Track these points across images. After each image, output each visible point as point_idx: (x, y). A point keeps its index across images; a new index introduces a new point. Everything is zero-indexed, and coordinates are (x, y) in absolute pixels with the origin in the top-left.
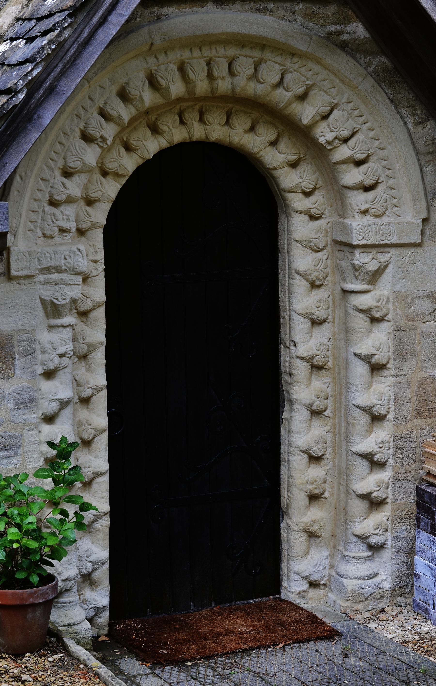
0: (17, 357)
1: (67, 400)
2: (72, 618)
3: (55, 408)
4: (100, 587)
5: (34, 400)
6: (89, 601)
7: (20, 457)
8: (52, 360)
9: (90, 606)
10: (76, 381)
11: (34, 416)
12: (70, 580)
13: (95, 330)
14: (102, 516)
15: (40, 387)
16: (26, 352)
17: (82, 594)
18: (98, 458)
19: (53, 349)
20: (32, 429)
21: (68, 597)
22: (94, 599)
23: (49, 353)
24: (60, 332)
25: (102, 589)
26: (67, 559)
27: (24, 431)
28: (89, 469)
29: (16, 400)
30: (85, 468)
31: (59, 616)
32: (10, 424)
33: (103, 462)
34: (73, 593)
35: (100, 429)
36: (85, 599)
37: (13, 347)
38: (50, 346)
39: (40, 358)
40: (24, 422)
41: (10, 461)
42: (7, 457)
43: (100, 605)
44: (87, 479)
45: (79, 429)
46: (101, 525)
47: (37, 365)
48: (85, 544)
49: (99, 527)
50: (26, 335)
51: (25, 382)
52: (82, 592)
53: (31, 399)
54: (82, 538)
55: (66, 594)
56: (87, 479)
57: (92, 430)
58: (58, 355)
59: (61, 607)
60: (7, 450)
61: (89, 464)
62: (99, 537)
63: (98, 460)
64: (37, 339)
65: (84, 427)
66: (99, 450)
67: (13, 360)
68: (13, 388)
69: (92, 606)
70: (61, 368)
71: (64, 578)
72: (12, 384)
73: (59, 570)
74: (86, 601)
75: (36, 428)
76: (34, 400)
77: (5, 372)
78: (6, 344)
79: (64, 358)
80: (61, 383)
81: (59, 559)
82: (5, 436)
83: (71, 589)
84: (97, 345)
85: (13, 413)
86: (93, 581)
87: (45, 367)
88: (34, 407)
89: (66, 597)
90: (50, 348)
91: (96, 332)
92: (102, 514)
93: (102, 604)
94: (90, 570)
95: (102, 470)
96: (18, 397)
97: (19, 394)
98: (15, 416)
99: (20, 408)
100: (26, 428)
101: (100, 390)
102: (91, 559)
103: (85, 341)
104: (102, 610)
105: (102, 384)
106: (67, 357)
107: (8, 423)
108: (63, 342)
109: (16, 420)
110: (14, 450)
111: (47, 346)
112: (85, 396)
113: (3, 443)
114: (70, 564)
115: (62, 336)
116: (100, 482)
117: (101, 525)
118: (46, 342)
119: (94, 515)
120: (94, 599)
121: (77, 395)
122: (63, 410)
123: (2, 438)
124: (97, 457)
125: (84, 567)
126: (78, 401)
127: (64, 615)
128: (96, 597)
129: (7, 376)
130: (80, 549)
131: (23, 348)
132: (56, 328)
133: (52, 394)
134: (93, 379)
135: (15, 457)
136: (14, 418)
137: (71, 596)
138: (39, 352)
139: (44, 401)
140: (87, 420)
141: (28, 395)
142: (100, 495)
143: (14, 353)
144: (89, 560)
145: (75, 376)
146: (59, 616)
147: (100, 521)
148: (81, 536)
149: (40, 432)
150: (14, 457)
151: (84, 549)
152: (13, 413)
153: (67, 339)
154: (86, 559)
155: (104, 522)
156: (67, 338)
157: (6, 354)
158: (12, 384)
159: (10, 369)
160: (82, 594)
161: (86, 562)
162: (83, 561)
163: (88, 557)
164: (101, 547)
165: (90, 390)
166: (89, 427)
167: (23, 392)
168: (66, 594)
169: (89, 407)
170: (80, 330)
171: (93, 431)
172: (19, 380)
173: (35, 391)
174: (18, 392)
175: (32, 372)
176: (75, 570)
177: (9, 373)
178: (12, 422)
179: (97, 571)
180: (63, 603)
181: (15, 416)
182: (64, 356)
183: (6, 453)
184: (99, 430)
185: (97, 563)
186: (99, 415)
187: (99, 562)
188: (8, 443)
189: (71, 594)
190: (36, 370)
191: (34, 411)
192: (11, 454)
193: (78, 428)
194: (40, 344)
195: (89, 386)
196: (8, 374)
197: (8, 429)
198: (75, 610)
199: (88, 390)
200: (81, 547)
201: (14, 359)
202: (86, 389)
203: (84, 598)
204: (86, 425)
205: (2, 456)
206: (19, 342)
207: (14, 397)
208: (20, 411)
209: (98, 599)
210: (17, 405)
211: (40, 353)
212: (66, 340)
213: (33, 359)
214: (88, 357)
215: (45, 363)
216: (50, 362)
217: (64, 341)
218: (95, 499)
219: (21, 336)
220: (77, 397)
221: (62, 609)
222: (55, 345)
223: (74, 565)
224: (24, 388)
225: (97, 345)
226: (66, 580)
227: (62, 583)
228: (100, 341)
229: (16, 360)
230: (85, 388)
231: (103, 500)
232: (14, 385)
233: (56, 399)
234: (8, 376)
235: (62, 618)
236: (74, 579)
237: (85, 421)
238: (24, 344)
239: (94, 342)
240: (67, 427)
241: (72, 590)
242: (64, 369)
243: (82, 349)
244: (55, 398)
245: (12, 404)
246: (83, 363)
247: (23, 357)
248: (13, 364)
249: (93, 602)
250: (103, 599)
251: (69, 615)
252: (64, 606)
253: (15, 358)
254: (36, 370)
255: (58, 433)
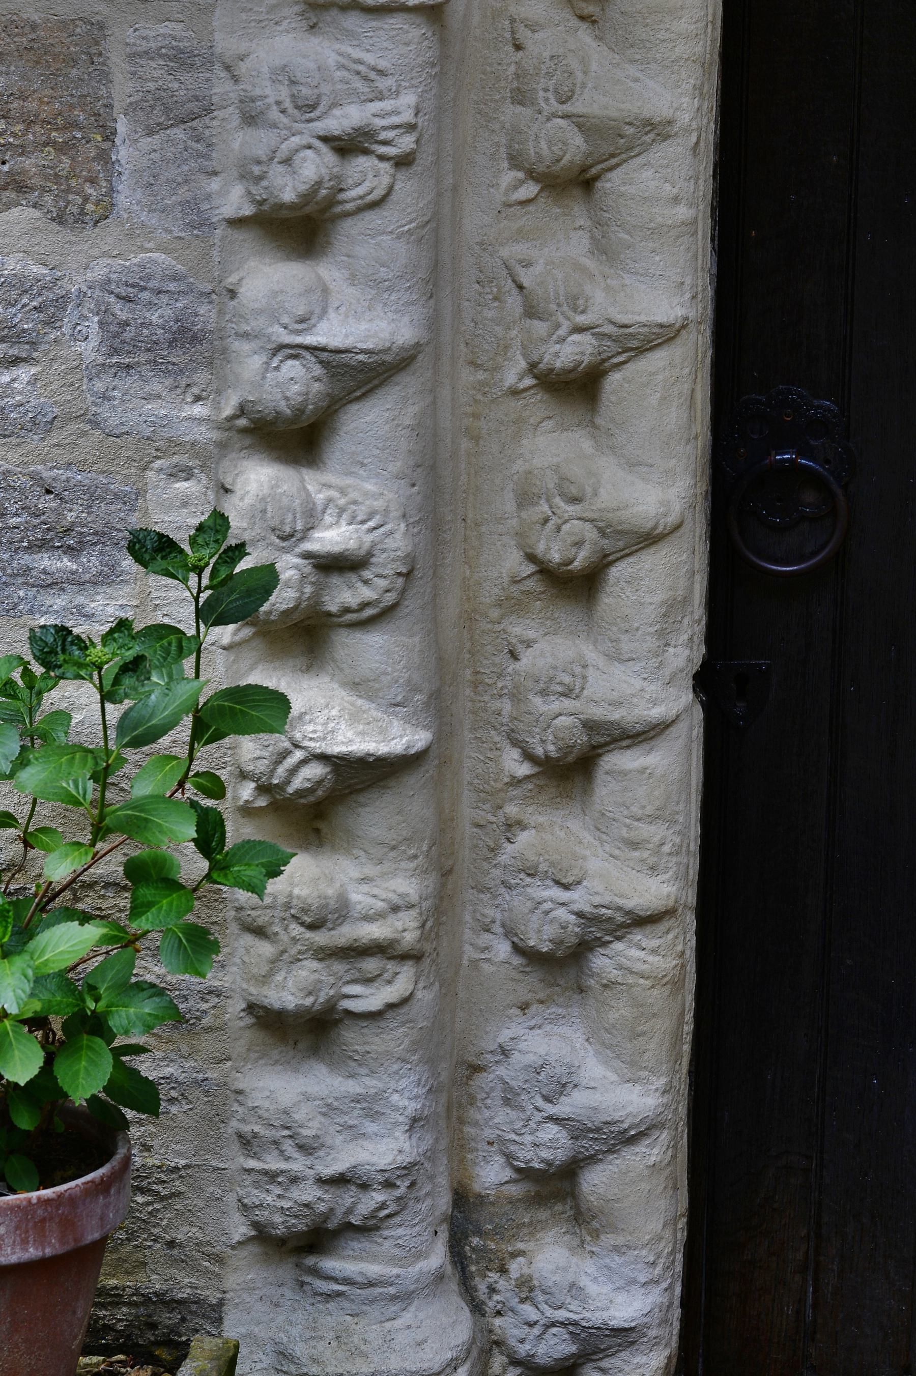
0: (122, 126)
1: (361, 357)
2: (364, 1355)
3: (296, 388)
4: (608, 1239)
5: (195, 339)
6: (544, 1292)
7: (127, 589)
8: (287, 161)
9: (549, 1312)
10: (521, 287)
11: (198, 410)
12: (365, 1187)
13: (633, 61)
14: (622, 926)
15: (232, 279)
16: (167, 110)
17: (522, 1253)
18: (622, 661)
19: (297, 107)
20: (187, 474)
21: (362, 1259)
22: (572, 1285)
23: (274, 126)
24: (350, 34)
25: (616, 1249)
26: (359, 1090)
27: (150, 474)
28: (568, 704)
29: (112, 328)
30: (544, 693)
31: (308, 1334)
32: (84, 434)
33: (638, 683)
34: (387, 1244)
35: (625, 527)
36: (530, 1278)
37: (105, 77)
38: (284, 93)
39: (236, 145)
40: (148, 431)
41: (80, 600)
42: (70, 582)
43: (596, 1318)
44: (551, 748)
45: (524, 515)
46: (620, 967)
47: (215, 173)
48: (548, 1035)
49: (615, 974)
50: (162, 29)
51: (157, 249)
52: (520, 1246)
53: (183, 330)
54: (534, 1008)
55: (356, 1245)
56: (551, 748)
57: (588, 526)
58: (325, 139)
59: (330, 1297)
60: (70, 550)
61: (567, 679)
62: (613, 1016)
63: (618, 670)
64: (218, 50)
65: (545, 508)
66: (625, 626)
67: (106, 139)
68: (98, 272)
69: (561, 1315)
70: (349, 207)
71: (328, 1171)
72: (96, 252)
73: (305, 1132)
74: (531, 1290)
75: (203, 468)
76: (195, 339)
77: (68, 190)
78: (73, 62)
79: (363, 163)
80: (352, 279)
81: (94, 1097)
82: (58, 487)
83: (377, 1228)
84: (630, 130)
85: (99, 385)
86: (583, 1207)
87: (258, 192)
88: (194, 370)
89: (355, 1258)
90: (278, 103)
91: (632, 70)
92: (619, 918)
93: (605, 1315)
94: (560, 1156)
95: (629, 718)
96: (123, 316)
97: (127, 299)
98: (105, 397)
99: (129, 367)
100: (158, 464)
101: (635, 344)
102: (562, 1108)
103: (567, 108)
104: (608, 1342)
105: (643, 318)
106: (382, 158)
107: (73, 427)
108: (359, 84)
109: (112, 417)
110: (101, 553)
111: (268, 91)
112: (558, 364)
113: (50, 517)
114: (373, 1115)
115: (356, 53)
116: (624, 773)
117: (620, 967)
118: (265, 70)
119: (580, 915)
120: (572, 1285)
121: (525, 356)
122: (354, 407)
123: (48, 492)
124: (616, 657)
125: (528, 1139)
126: (529, 381)
127: (332, 1335)
128: (584, 1281)
129: (75, 210)
130: (516, 1057)
131: (151, 86)
132: (334, 12)
133: (285, 320)
134: (608, 289)
135: (104, 588)
136: (104, 411)
137: (374, 1258)
138: (232, 115)
139: (245, 347)
140: (562, 479)
141: (168, 312)
142: (624, 832)
143: (110, 106)
144: (550, 1109)
145: (512, 262)
146: (308, 1334)
147: (618, 946)
148: (524, 995)
149: (227, 491)
150: (101, 589)
151: (530, 1059)
152: (99, 385)
153: (381, 73)
154: (540, 1102)
155: (634, 953)
156: (382, 64)
157: (72, 107)
158: (96, 252)
159: (93, 181)
160: (522, 1253)
161: (538, 1116)
162: (522, 1109)
163: (547, 1099)
164: (617, 1064)
165: (586, 339)
166: (572, 510)
167: (145, 295)
168: (355, 1245)
169: (599, 421)
170: (546, 54)
171: (590, 533)
172: (130, 235)
173: (202, 294)
174: (122, 291)
175: (191, 205)
176: (394, 1145)
177: (86, 199)
178: (95, 424)
179: (599, 1167)
180: (335, 1280)
181: (105, 397)
182: (366, 152)
183: (67, 563)
184: (620, 532)
185: (590, 1130)
186: (632, 465)
187: (598, 1130)
188: (70, 517)
189: (375, 1248)
190: (208, 198)
191: (195, 390)
192: (86, 570)
193: (520, 506)
194: (236, 79)
195: (581, 319)
196: (80, 200)
197: (77, 455)
198: (398, 1323)
199: (576, 337)
200: (522, 1046)
201: (110, 136)
202: (562, 332)
203: (526, 1271)
204: (558, 500)
205: (44, 572)
206: (132, 56)
207: (104, 312)
208: (130, 382)
209: (592, 1289)
210: (115, 351)
211: (236, 121)
212: (372, 75)
213: (199, 146)
214: (599, 184)
215: (257, 170)
216: (281, 169)
217: (366, 79)
218: (602, 842)
219: (145, 33)
220: (523, 364)
221: (332, 1305)
222: (305, 91)
223: (396, 1124)
224: (149, 278)
225: (630, 130)
226: (340, 1181)
227: (319, 1193)
228: (646, 114)
229: (118, 141)
230: (558, 326)
231: (636, 854)
232: (105, 254)
233: (307, 348)
234: (82, 213)
235: (321, 1345)
236: (389, 1185)
237: (551, 483)
238: (154, 69)
239: (614, 114)
240: (369, 487)
241: (386, 1233)
242: (370, 215)
243: (550, 143)
244: (299, 340)
245: (93, 342)
246: (579, 214)
247: (150, 133)
248: (104, 157)
249: (561, 1297)
250: (621, 1298)
251: (356, 1339)
252: (339, 1294)
253: (114, 133)
254: (208, 198)
255: (326, 507)
